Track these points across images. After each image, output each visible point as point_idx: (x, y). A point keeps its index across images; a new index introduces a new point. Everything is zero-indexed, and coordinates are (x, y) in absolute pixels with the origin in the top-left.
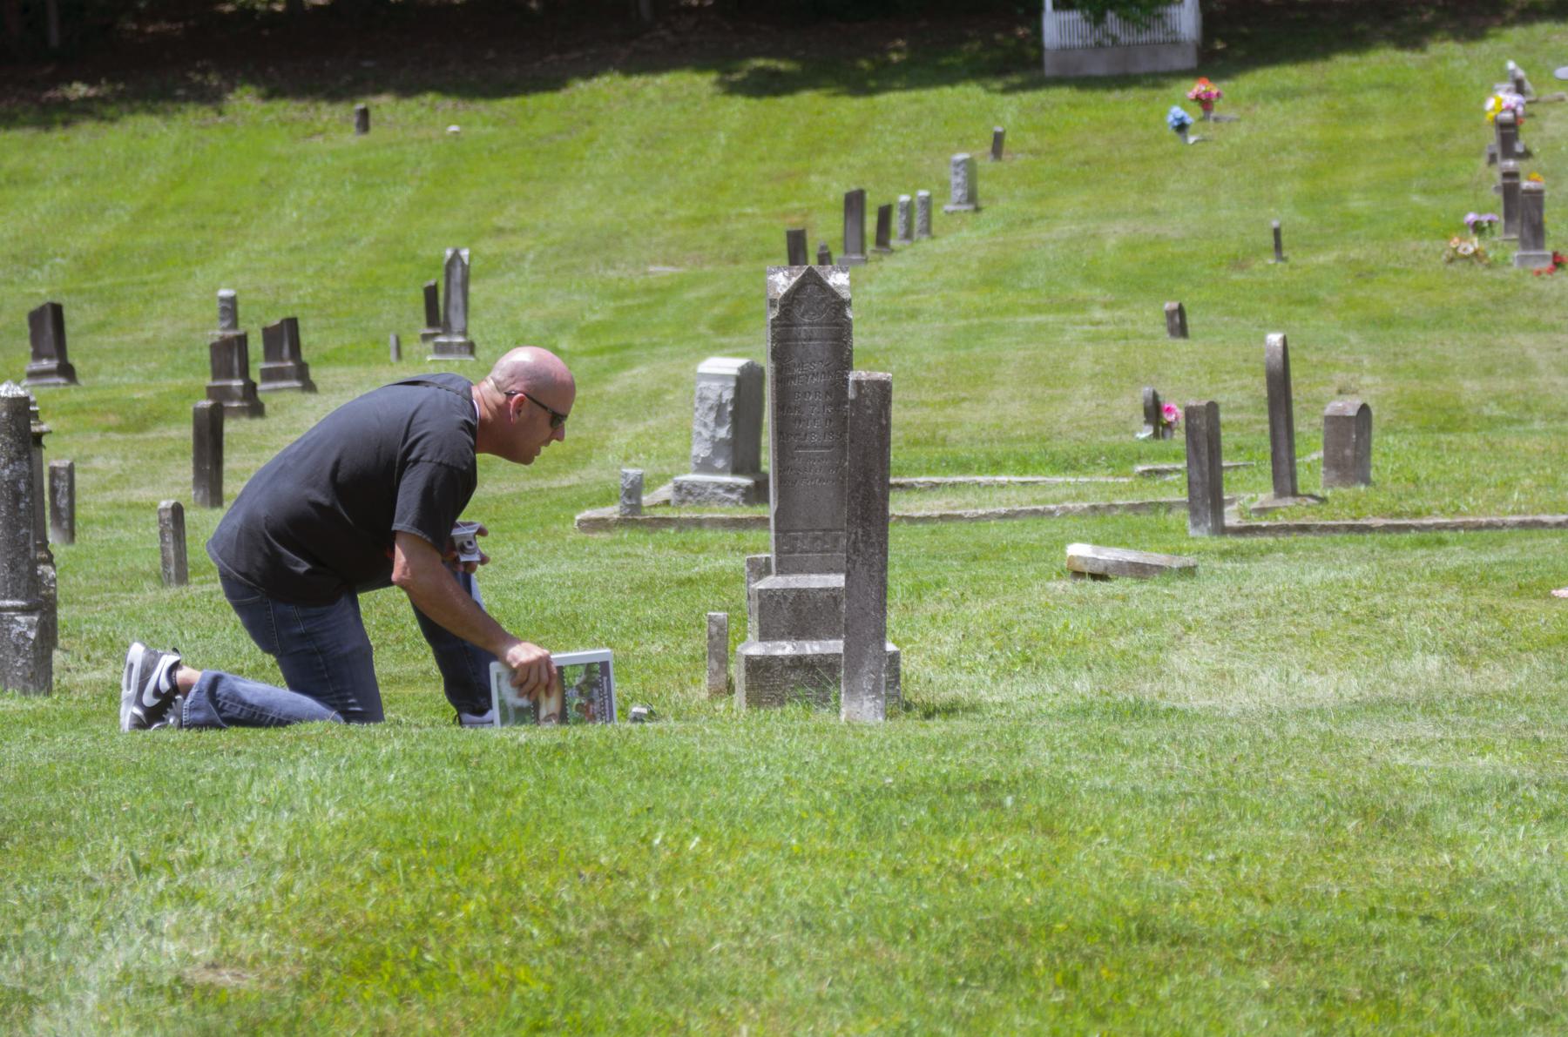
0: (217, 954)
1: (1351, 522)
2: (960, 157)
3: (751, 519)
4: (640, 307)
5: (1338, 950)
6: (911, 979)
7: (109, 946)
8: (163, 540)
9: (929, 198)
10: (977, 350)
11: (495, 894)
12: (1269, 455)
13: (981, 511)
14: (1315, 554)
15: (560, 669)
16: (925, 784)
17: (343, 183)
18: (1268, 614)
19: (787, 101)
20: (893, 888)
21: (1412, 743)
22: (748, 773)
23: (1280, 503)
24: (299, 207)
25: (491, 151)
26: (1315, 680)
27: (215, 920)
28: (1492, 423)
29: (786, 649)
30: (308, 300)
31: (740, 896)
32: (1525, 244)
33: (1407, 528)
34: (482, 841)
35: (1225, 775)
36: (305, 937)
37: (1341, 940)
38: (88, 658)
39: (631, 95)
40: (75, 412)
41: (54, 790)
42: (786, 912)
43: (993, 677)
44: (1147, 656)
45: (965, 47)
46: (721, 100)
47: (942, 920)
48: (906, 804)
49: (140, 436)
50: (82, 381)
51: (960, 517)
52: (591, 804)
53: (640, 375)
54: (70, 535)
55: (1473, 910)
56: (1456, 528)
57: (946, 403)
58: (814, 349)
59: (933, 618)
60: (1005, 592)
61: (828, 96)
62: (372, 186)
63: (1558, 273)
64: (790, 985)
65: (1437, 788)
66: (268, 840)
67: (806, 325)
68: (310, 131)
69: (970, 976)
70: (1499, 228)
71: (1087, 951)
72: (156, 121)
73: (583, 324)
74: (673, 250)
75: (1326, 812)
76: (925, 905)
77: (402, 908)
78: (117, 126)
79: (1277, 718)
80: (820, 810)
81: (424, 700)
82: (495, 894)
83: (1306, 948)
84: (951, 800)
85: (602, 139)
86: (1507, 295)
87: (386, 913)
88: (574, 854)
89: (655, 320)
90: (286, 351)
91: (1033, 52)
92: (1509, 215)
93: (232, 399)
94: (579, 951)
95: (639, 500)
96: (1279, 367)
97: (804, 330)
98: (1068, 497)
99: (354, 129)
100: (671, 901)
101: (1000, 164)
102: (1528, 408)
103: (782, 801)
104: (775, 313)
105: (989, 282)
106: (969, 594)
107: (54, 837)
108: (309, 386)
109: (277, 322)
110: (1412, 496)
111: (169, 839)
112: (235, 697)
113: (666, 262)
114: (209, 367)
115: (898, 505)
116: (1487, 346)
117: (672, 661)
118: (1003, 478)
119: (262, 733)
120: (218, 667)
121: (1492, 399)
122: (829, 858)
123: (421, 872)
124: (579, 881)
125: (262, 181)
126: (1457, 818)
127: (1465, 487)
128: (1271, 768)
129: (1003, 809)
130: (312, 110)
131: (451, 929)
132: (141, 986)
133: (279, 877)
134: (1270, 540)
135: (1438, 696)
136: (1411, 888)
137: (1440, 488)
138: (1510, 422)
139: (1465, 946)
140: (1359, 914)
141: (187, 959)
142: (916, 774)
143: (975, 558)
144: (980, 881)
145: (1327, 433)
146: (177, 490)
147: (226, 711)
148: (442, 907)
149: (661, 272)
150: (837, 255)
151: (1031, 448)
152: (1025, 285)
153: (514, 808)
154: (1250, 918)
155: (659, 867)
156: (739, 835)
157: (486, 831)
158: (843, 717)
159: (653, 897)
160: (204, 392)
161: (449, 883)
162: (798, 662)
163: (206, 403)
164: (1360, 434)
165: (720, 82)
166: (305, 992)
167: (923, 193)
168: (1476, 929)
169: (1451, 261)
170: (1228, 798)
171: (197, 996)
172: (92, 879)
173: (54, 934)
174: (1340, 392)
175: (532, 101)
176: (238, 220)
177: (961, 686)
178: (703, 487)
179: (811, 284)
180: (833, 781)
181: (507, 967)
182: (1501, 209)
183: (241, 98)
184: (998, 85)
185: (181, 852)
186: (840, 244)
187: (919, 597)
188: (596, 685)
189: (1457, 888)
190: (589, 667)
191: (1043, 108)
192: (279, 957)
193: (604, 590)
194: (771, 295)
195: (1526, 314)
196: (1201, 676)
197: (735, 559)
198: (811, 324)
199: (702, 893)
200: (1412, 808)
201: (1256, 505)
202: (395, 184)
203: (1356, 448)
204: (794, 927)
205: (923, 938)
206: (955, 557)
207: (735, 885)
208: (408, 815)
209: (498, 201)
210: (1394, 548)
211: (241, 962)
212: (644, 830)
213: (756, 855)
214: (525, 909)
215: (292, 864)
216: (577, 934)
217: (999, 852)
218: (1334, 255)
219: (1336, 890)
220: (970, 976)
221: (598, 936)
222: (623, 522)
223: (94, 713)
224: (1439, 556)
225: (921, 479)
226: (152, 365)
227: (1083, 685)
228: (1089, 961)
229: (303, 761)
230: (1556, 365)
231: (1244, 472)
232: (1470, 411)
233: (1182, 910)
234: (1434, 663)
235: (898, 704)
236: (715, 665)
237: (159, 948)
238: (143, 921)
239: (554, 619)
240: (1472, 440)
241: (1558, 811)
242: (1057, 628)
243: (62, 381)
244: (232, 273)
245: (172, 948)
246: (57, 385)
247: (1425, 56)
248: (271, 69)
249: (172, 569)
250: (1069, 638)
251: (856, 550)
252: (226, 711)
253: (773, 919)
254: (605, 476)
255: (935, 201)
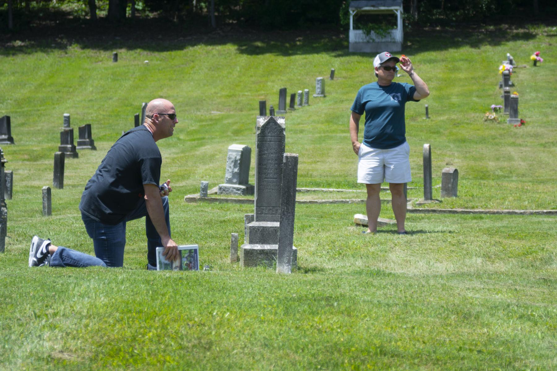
0: (63, 347)
1: (450, 210)
2: (319, 78)
3: (245, 200)
4: (208, 125)
5: (449, 361)
6: (302, 365)
7: (25, 343)
8: (43, 200)
9: (308, 92)
10: (323, 145)
11: (159, 330)
12: (423, 185)
13: (323, 201)
14: (438, 220)
15: (180, 251)
16: (306, 297)
17: (108, 78)
18: (423, 241)
19: (261, 57)
20: (296, 333)
21: (473, 289)
22: (245, 290)
23: (426, 202)
24: (92, 86)
25: (159, 70)
26: (438, 265)
27: (62, 335)
28: (499, 177)
29: (258, 247)
30: (94, 118)
31: (243, 334)
32: (511, 116)
33: (469, 212)
34: (154, 311)
35: (409, 298)
36: (93, 343)
37: (450, 358)
38: (17, 240)
39: (208, 53)
40: (13, 154)
41: (7, 287)
42: (259, 340)
43: (328, 259)
44: (382, 254)
45: (323, 40)
46: (238, 55)
47: (313, 345)
48: (300, 304)
49: (35, 163)
50: (15, 143)
51: (316, 202)
52: (192, 300)
53: (208, 149)
54: (11, 196)
55: (495, 349)
56: (486, 213)
57: (312, 163)
58: (272, 145)
59: (308, 238)
60: (333, 230)
61: (275, 55)
62: (118, 80)
63: (522, 126)
64: (260, 366)
65: (482, 305)
66: (81, 308)
67: (270, 136)
68: (97, 60)
69: (322, 365)
70: (502, 110)
71: (363, 358)
72: (44, 55)
73: (189, 130)
74: (220, 106)
75: (444, 312)
76: (307, 340)
77: (127, 334)
78: (31, 56)
79: (426, 278)
80: (271, 305)
81: (133, 259)
82: (159, 330)
83: (438, 360)
84: (316, 303)
85: (197, 67)
86: (505, 133)
87: (121, 335)
88: (186, 317)
89: (213, 130)
90: (86, 136)
91: (345, 43)
92: (506, 106)
93: (67, 152)
94: (188, 352)
95: (207, 192)
96: (428, 155)
97: (269, 138)
98: (353, 197)
99: (112, 60)
100: (219, 335)
101: (333, 81)
102: (511, 172)
103: (257, 301)
104: (259, 132)
105: (328, 121)
106: (320, 230)
107: (7, 304)
108: (94, 148)
109: (84, 125)
110: (471, 201)
111: (47, 306)
112: (69, 256)
113: (217, 110)
114: (60, 140)
115: (299, 198)
116: (497, 150)
117: (218, 249)
118: (331, 189)
119: (78, 269)
120: (62, 245)
121: (499, 169)
122: (273, 322)
123: (133, 321)
124: (187, 327)
125: (80, 77)
126: (489, 316)
127: (490, 199)
128: (425, 296)
129: (334, 307)
130: (98, 53)
131: (144, 342)
132: (36, 358)
133: (85, 321)
134: (423, 215)
135: (481, 272)
136: (474, 340)
137: (481, 199)
138: (505, 177)
139: (492, 361)
140: (456, 349)
141: (52, 349)
142: (304, 293)
143: (322, 217)
144: (326, 332)
145: (443, 179)
146: (48, 182)
147: (65, 261)
148: (141, 334)
149: (216, 113)
150: (276, 110)
151: (341, 179)
152: (340, 123)
153: (166, 300)
154: (418, 349)
155: (216, 323)
156: (243, 313)
157: (156, 307)
158: (277, 271)
159: (213, 333)
160: (58, 149)
161: (143, 325)
162: (262, 252)
163: (59, 153)
164: (454, 179)
165: (238, 49)
166: (93, 362)
167: (306, 90)
168: (496, 356)
169: (486, 121)
170: (411, 306)
171: (56, 362)
172: (20, 320)
173: (6, 338)
174: (447, 164)
175: (174, 53)
176: (71, 90)
177: (316, 262)
178: (228, 188)
179: (272, 122)
180: (275, 295)
181: (163, 356)
182: (504, 104)
183: (74, 48)
184: (333, 54)
185: (50, 311)
186: (278, 106)
187: (304, 230)
188: (193, 257)
189: (490, 341)
190: (190, 251)
191: (348, 63)
192: (84, 349)
193: (195, 223)
194: (258, 125)
195: (511, 140)
196: (399, 262)
197: (241, 214)
198: (271, 137)
199: (231, 333)
200: (474, 312)
201: (418, 202)
202: (126, 79)
203: (453, 184)
204: (261, 345)
205: (306, 351)
206: (315, 216)
207: (241, 330)
208: (129, 301)
209: (161, 87)
210: (465, 219)
211: (71, 351)
212: (210, 310)
213: (249, 320)
214: (169, 336)
215: (89, 317)
216: (187, 345)
217: (332, 322)
218: (446, 117)
219: (448, 340)
220: (322, 365)
221: (194, 346)
222: (201, 199)
223: (19, 260)
224: (481, 223)
225: (303, 189)
226: (40, 139)
227: (359, 263)
228: (363, 362)
229: (92, 280)
230: (521, 158)
231: (414, 191)
232: (491, 173)
233: (395, 345)
234: (479, 260)
235: (296, 267)
236: (233, 251)
237: (43, 344)
238: (37, 335)
239: (177, 233)
240: (492, 183)
241: (524, 315)
242: (351, 243)
243: (9, 143)
244: (68, 108)
245: (47, 344)
246: (7, 144)
247: (479, 50)
248: (84, 39)
249: (46, 210)
250: (355, 247)
251: (284, 214)
252: (65, 261)
253: (254, 342)
254: (195, 183)
255: (310, 93)
